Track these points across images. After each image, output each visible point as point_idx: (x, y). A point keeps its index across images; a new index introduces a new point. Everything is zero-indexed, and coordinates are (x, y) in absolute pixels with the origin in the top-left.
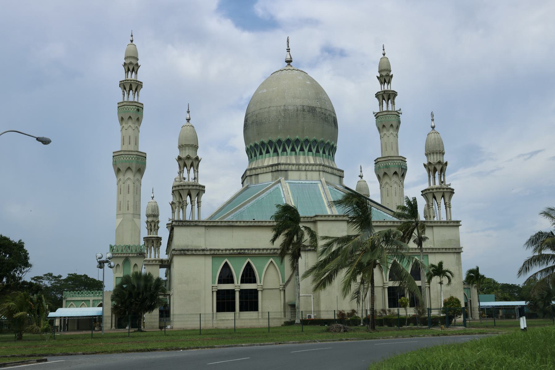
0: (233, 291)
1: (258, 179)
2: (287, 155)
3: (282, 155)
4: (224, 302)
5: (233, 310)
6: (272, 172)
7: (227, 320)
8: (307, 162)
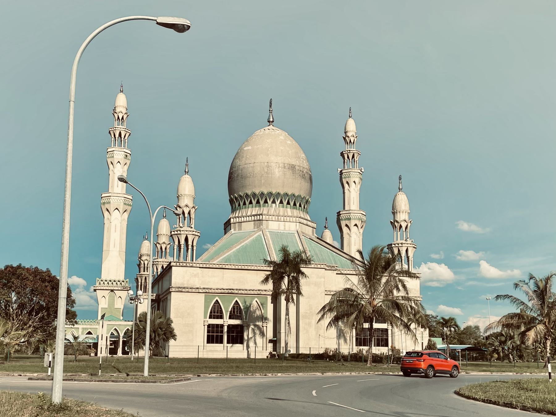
0: (222, 326)
1: (241, 226)
2: (268, 206)
3: (264, 206)
4: (214, 336)
5: (221, 342)
6: (254, 221)
7: (218, 351)
8: (286, 214)
